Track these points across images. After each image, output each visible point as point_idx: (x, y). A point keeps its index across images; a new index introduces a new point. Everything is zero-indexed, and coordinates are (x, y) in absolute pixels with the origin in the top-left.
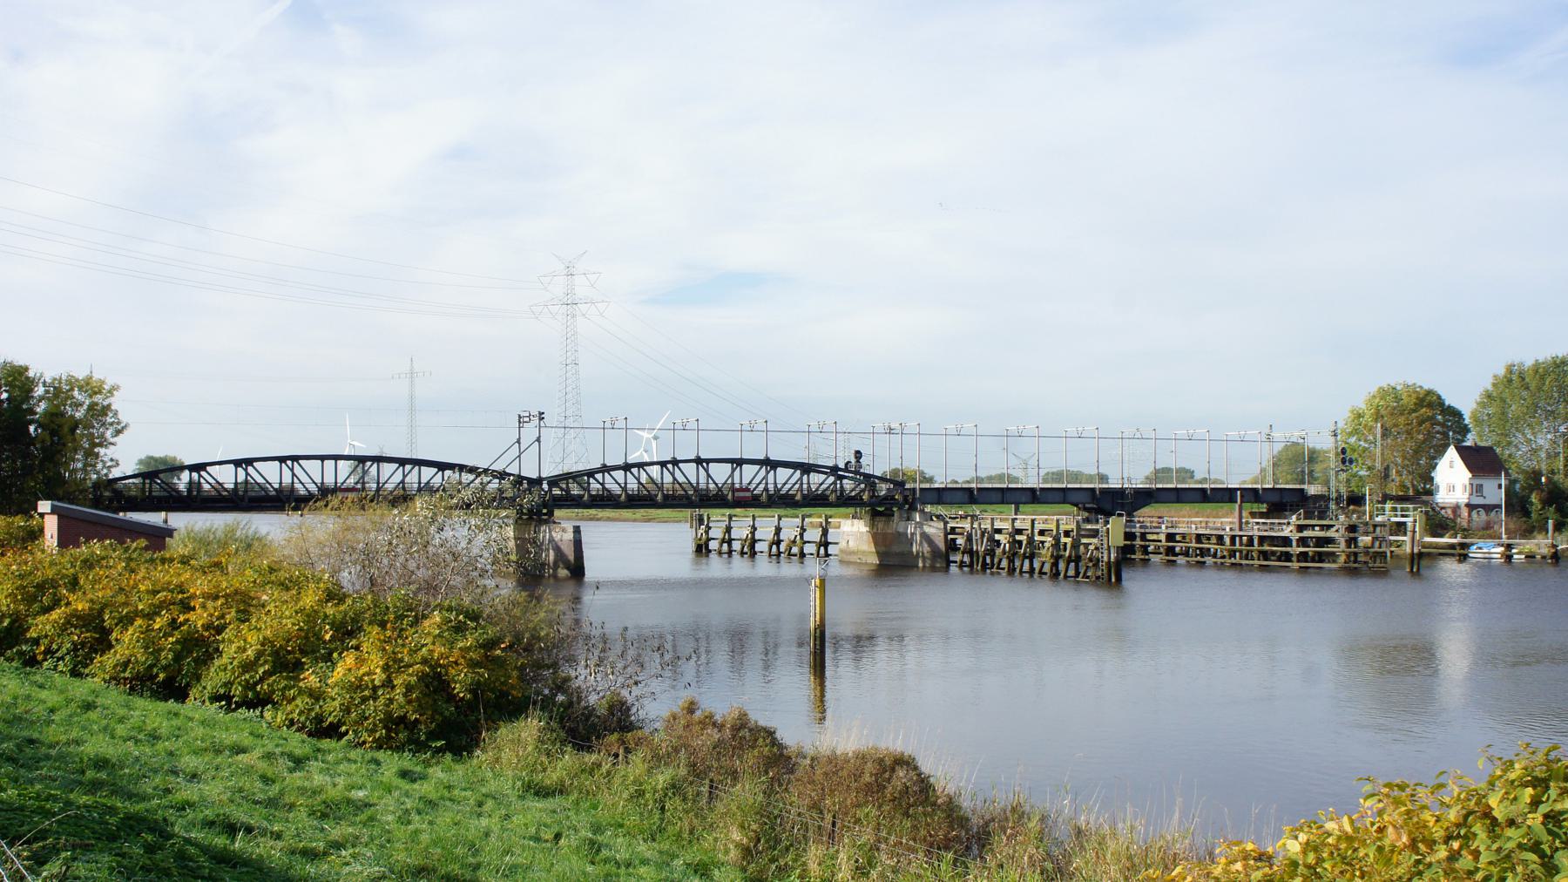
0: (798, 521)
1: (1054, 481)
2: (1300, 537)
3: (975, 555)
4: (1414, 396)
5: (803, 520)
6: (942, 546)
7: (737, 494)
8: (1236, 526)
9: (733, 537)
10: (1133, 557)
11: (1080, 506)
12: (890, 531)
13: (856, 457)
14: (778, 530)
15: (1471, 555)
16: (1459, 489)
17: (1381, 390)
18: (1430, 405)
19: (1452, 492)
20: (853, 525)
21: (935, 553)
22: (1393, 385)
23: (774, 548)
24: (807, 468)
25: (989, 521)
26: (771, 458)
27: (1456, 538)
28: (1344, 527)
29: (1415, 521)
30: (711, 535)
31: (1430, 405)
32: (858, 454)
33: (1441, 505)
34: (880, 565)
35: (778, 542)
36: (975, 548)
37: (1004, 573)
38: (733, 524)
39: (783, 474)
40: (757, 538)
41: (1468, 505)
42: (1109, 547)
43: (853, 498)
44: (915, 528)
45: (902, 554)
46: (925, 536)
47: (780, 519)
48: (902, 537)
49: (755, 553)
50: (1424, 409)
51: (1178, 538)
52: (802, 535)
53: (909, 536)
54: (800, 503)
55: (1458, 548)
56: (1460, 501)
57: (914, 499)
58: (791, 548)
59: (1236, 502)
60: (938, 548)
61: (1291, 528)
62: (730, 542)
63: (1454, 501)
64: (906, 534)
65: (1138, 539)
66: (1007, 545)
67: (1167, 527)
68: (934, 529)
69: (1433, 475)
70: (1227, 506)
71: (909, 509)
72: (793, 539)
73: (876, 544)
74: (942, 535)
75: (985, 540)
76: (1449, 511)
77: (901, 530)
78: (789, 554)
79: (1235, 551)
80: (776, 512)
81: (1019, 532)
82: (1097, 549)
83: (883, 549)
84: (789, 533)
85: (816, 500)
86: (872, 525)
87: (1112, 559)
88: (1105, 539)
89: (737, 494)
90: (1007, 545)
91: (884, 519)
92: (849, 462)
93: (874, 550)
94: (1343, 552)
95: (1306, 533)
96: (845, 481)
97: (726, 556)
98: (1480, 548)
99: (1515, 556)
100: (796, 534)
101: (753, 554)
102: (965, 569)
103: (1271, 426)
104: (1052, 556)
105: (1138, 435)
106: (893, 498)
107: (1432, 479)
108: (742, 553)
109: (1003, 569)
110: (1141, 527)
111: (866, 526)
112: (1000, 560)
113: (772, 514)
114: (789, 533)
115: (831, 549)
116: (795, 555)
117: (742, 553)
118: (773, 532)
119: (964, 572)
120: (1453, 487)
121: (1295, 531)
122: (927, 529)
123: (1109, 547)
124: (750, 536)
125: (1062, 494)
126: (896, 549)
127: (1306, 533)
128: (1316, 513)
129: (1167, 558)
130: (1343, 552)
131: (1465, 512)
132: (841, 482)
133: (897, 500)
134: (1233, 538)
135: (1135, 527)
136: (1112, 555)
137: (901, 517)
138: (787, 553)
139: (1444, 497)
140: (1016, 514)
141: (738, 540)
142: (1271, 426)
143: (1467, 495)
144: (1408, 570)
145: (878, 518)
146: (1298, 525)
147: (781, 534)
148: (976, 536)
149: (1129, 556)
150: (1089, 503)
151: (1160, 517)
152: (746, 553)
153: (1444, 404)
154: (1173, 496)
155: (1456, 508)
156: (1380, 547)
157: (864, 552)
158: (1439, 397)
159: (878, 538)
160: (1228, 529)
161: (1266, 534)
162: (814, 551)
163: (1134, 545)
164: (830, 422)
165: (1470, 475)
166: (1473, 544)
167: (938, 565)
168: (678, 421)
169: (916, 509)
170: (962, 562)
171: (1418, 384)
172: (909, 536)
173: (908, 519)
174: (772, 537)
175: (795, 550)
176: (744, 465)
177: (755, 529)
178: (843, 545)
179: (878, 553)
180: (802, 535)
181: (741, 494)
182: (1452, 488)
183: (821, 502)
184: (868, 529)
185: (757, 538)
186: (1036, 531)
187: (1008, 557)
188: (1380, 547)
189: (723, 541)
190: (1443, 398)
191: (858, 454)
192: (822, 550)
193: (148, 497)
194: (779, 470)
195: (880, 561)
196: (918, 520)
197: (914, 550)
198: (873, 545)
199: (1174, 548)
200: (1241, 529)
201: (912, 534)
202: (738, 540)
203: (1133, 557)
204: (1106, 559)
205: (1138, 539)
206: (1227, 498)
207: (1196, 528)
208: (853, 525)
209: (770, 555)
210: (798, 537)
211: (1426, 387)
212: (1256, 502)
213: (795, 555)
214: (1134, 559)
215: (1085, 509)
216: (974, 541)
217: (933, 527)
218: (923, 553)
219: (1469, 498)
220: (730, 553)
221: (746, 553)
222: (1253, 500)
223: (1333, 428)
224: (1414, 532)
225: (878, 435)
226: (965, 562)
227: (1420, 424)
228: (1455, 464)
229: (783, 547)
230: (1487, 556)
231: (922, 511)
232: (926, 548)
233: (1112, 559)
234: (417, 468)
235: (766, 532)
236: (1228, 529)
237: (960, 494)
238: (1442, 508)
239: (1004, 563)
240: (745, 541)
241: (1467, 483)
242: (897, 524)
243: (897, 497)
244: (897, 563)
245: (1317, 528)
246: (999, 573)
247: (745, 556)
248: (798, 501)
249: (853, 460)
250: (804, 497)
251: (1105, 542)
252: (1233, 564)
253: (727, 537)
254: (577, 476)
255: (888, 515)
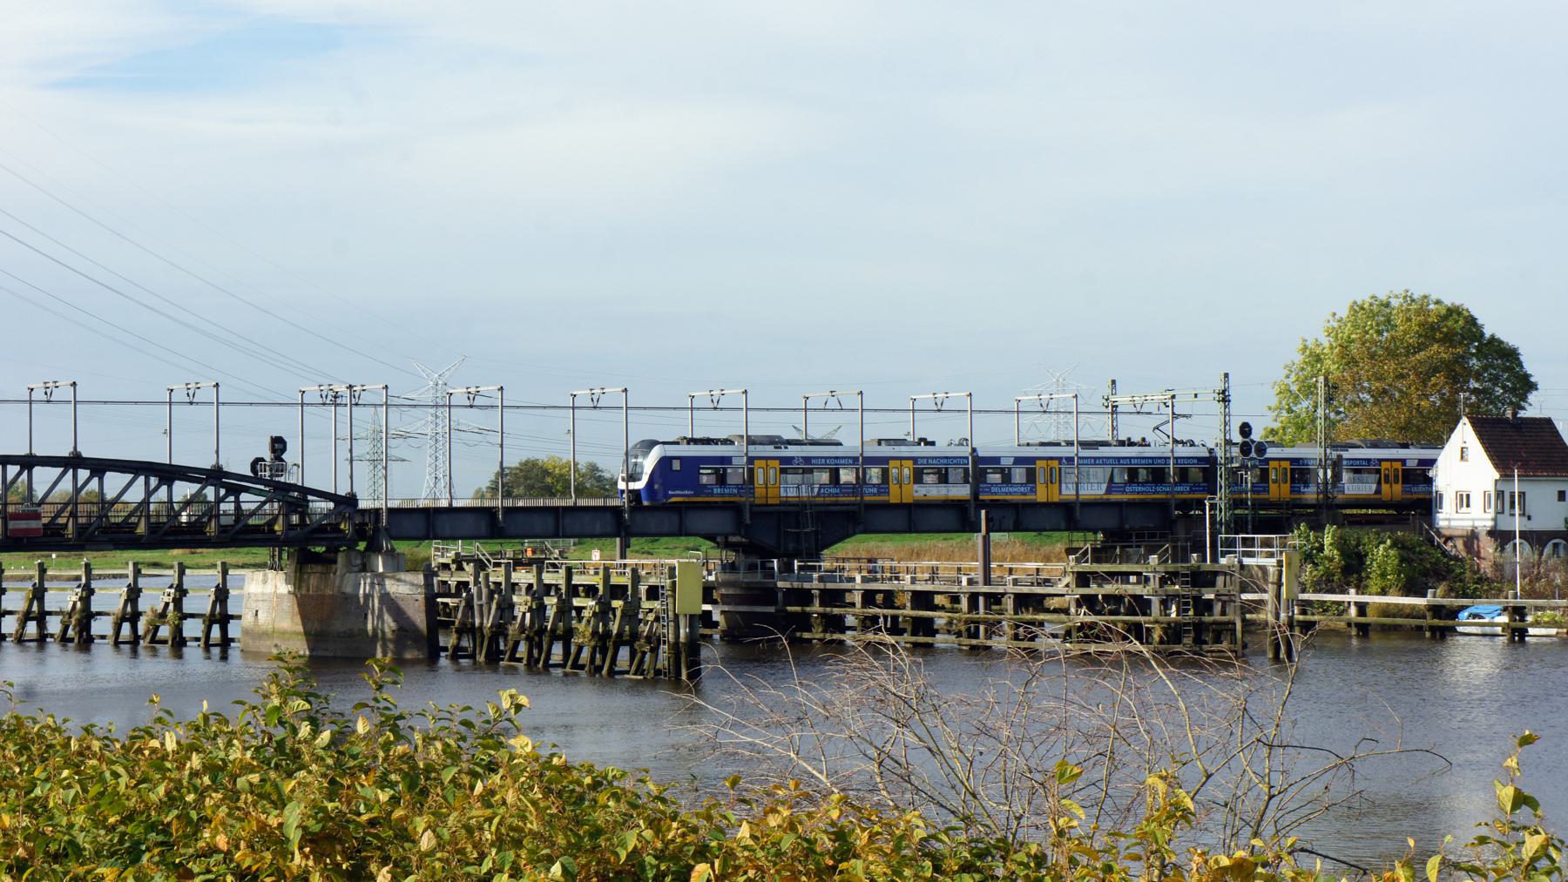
0: (172, 574)
1: (531, 491)
2: (1082, 596)
3: (478, 635)
4: (1415, 320)
5: (182, 573)
6: (419, 618)
7: (12, 525)
8: (979, 577)
9: (47, 608)
10: (806, 635)
11: (719, 539)
12: (329, 592)
13: (273, 450)
14: (134, 594)
15: (1460, 629)
16: (1477, 501)
17: (1357, 309)
18: (1449, 339)
19: (1464, 509)
20: (265, 582)
21: (405, 630)
22: (1383, 297)
23: (126, 629)
24: (168, 474)
25: (562, 572)
26: (84, 455)
27: (1424, 596)
28: (1158, 576)
29: (1280, 563)
30: (187, 608)
31: (1449, 339)
32: (278, 445)
33: (1447, 533)
34: (311, 657)
35: (134, 618)
36: (477, 622)
37: (521, 666)
38: (142, 582)
39: (114, 482)
40: (94, 609)
41: (1492, 533)
42: (676, 616)
43: (257, 528)
44: (372, 585)
45: (350, 635)
46: (389, 602)
47: (137, 573)
48: (353, 606)
49: (90, 640)
50: (1436, 346)
51: (879, 597)
52: (178, 602)
53: (362, 600)
54: (143, 541)
55: (1428, 614)
56: (1477, 524)
57: (376, 530)
58: (157, 629)
59: (980, 531)
60: (413, 625)
61: (1068, 579)
62: (41, 618)
63: (1468, 525)
64: (357, 596)
65: (817, 602)
66: (528, 615)
67: (864, 580)
68: (406, 588)
69: (1431, 474)
70: (958, 539)
71: (367, 549)
72: (160, 611)
73: (305, 616)
74: (421, 598)
75: (494, 606)
76: (1460, 544)
77: (348, 590)
78: (153, 641)
79: (977, 622)
80: (217, 556)
81: (547, 589)
82: (657, 619)
83: (317, 626)
84: (154, 597)
85: (191, 536)
86: (298, 580)
87: (682, 638)
88: (670, 600)
89: (12, 525)
90: (528, 615)
91: (319, 568)
92: (258, 460)
93: (300, 628)
94: (1156, 622)
95: (1093, 589)
96: (244, 497)
97: (126, 648)
98: (1475, 616)
99: (1531, 631)
100: (166, 599)
101: (86, 642)
102: (463, 661)
103: (1114, 382)
104: (595, 633)
105: (833, 404)
106: (335, 528)
107: (1429, 481)
108: (64, 639)
109: (520, 660)
110: (821, 579)
111: (287, 582)
112: (517, 644)
113: (207, 561)
114: (154, 597)
115: (234, 630)
116: (164, 642)
117: (64, 639)
118: (124, 597)
119: (460, 670)
120: (1468, 496)
121: (1073, 586)
122: (392, 587)
123: (676, 616)
124: (79, 605)
125: (550, 520)
126: (339, 626)
127: (1093, 589)
128: (1118, 551)
129: (914, 639)
130: (1156, 622)
131: (1488, 548)
132: (237, 498)
133: (343, 531)
134: (973, 598)
135: (810, 580)
136: (682, 631)
137: (349, 566)
138: (149, 638)
139: (1449, 518)
140: (623, 556)
141: (57, 613)
142: (1114, 382)
143: (1491, 513)
144: (1270, 655)
145: (309, 568)
146: (1078, 573)
147: (229, 601)
148: (480, 598)
149: (798, 634)
150: (734, 534)
151: (870, 561)
152: (71, 640)
153: (1482, 334)
154: (951, 517)
155: (1471, 538)
156: (1223, 613)
157: (284, 633)
158: (1472, 321)
159: (307, 606)
160: (964, 583)
161: (1025, 590)
162: (109, 631)
163: (809, 615)
164: (64, 382)
165: (1497, 476)
166: (1463, 608)
167: (408, 656)
168: (179, 388)
169: (379, 550)
170: (457, 648)
171: (1434, 297)
172: (362, 600)
173: (364, 568)
174: (121, 605)
175: (165, 632)
176: (108, 474)
177: (91, 592)
178: (248, 619)
179: (307, 633)
180: (178, 602)
181: (22, 524)
182: (1464, 500)
183: (188, 537)
184: (290, 588)
185: (94, 609)
186: (643, 589)
187: (528, 639)
188: (1223, 613)
189: (27, 617)
190: (1480, 322)
191: (278, 445)
192: (216, 632)
193: (797, 554)
194: (37, 470)
195: (311, 650)
196: (381, 570)
197: (370, 627)
198: (298, 619)
199: (841, 618)
200: (987, 581)
201: (367, 596)
202: (57, 613)
203: (806, 635)
204: (671, 638)
205: (817, 602)
206: (1010, 522)
207: (913, 581)
208: (265, 582)
209: (117, 643)
210: (171, 606)
211: (1448, 302)
212: (1068, 529)
213: (164, 642)
214: (809, 641)
215: (728, 546)
216: (476, 607)
217: (405, 581)
218: (383, 632)
219: (1495, 520)
220: (42, 639)
221: (71, 640)
222: (1063, 525)
223: (1221, 387)
224: (1279, 584)
225: (700, 412)
226: (465, 649)
227: (1424, 378)
228: (1470, 453)
229: (142, 626)
230: (1488, 630)
231: (391, 554)
232: (389, 624)
233: (682, 638)
234: (142, 479)
235: (110, 597)
236: (858, 579)
237: (470, 518)
238: (1449, 538)
239: (523, 649)
240: (70, 615)
241: (1491, 488)
242: (343, 576)
243: (342, 526)
244: (339, 654)
245: (1133, 579)
246: (576, 674)
247: (70, 645)
248: (141, 536)
249: (267, 455)
250: (154, 528)
251: (671, 607)
252: (973, 648)
253: (35, 608)
254: (6, 486)
255: (327, 561)
